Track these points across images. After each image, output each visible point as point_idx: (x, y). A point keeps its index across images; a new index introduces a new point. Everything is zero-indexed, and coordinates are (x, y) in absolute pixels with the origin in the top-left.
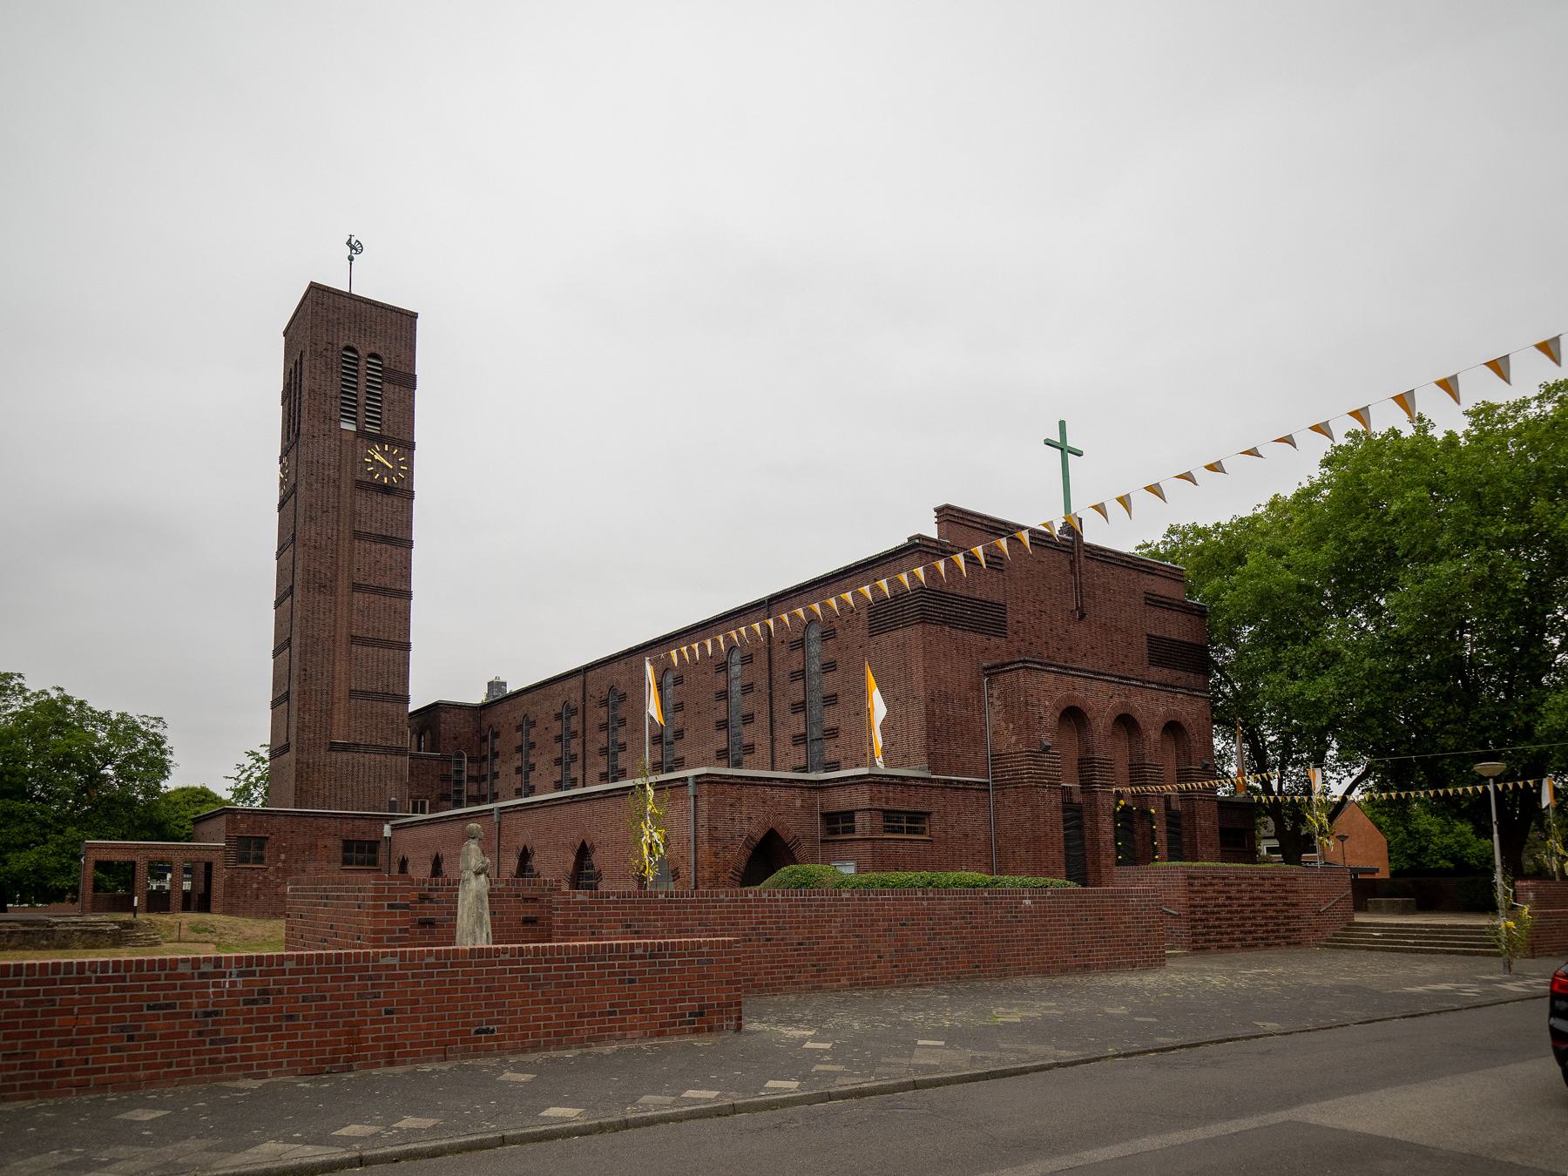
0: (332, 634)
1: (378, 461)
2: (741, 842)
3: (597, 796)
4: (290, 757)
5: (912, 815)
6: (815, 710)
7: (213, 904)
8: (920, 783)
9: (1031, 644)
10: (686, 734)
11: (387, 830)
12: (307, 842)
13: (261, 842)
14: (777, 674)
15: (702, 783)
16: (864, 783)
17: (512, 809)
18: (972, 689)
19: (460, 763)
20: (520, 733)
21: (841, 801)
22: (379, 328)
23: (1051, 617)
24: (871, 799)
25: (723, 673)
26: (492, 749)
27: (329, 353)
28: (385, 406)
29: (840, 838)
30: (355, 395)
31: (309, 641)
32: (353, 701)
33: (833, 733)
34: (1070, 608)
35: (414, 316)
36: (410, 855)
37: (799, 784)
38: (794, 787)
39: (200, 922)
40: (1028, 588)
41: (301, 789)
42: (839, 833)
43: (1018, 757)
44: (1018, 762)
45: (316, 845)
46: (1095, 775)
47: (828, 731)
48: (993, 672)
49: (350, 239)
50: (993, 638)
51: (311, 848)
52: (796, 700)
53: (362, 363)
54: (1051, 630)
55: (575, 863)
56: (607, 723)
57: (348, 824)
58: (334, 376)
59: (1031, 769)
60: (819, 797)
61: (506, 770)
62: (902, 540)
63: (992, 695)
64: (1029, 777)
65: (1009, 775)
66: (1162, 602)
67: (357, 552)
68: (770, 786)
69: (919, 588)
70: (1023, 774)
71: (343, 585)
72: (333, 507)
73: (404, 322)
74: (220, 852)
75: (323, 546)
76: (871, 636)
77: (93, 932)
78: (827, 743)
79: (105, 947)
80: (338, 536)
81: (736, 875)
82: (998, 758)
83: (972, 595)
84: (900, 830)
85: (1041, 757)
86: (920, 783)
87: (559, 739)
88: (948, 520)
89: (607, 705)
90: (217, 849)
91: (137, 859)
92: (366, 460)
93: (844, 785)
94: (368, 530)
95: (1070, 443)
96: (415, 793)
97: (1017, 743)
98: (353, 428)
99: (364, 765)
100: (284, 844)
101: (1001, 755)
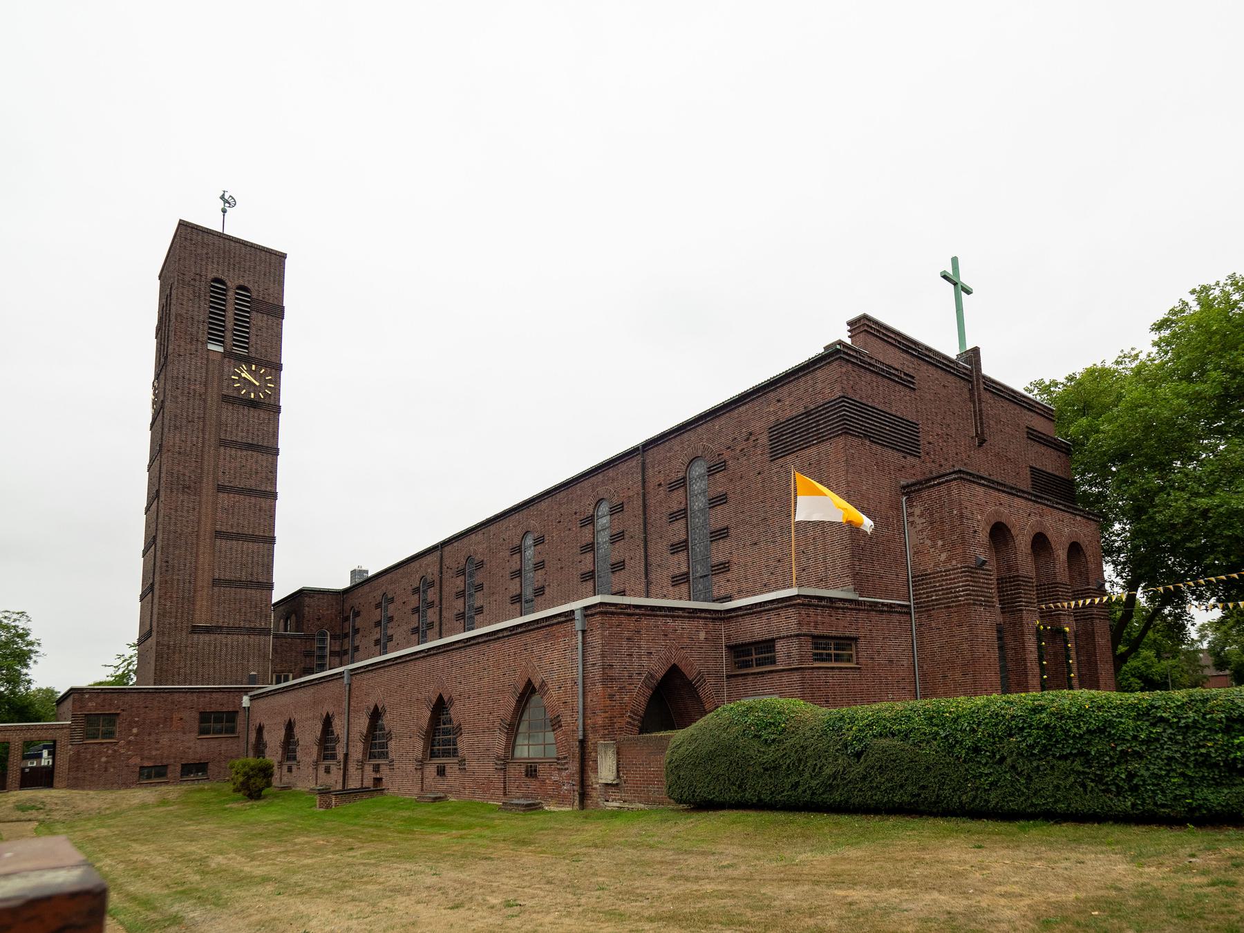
0: (196, 529)
1: (245, 378)
2: (639, 682)
3: (457, 646)
4: (152, 641)
5: (842, 642)
6: (698, 548)
7: (56, 780)
8: (847, 605)
9: (941, 466)
10: (547, 590)
11: (246, 701)
13: (111, 718)
14: (653, 517)
15: (592, 615)
16: (789, 606)
17: (363, 670)
19: (324, 641)
20: (379, 610)
21: (756, 629)
22: (248, 264)
23: (956, 441)
24: (799, 623)
25: (590, 527)
26: (353, 627)
27: (197, 283)
29: (753, 671)
30: (223, 321)
31: (172, 536)
32: (216, 589)
33: (724, 567)
35: (283, 256)
36: (267, 723)
37: (703, 615)
38: (698, 618)
39: (31, 799)
40: (936, 411)
41: (161, 669)
43: (950, 575)
44: (951, 579)
46: (1021, 593)
47: (717, 566)
48: (910, 491)
49: (224, 195)
50: (909, 457)
52: (676, 540)
53: (231, 293)
54: (957, 454)
55: (431, 719)
56: (464, 591)
58: (202, 304)
59: (969, 585)
60: (723, 628)
62: (820, 350)
64: (967, 595)
65: (936, 595)
66: (1040, 438)
67: (222, 457)
68: (673, 617)
69: (840, 398)
70: (959, 592)
71: (208, 487)
72: (199, 418)
73: (275, 261)
74: (65, 731)
75: (188, 452)
76: (772, 461)
78: (715, 579)
80: (203, 443)
81: (634, 720)
82: (921, 579)
84: (828, 658)
85: (977, 573)
86: (847, 605)
88: (865, 330)
89: (464, 574)
90: (62, 727)
92: (233, 377)
93: (761, 611)
94: (234, 439)
95: (964, 279)
96: (278, 668)
97: (949, 559)
98: (221, 349)
99: (226, 645)
100: (136, 719)
101: (926, 575)
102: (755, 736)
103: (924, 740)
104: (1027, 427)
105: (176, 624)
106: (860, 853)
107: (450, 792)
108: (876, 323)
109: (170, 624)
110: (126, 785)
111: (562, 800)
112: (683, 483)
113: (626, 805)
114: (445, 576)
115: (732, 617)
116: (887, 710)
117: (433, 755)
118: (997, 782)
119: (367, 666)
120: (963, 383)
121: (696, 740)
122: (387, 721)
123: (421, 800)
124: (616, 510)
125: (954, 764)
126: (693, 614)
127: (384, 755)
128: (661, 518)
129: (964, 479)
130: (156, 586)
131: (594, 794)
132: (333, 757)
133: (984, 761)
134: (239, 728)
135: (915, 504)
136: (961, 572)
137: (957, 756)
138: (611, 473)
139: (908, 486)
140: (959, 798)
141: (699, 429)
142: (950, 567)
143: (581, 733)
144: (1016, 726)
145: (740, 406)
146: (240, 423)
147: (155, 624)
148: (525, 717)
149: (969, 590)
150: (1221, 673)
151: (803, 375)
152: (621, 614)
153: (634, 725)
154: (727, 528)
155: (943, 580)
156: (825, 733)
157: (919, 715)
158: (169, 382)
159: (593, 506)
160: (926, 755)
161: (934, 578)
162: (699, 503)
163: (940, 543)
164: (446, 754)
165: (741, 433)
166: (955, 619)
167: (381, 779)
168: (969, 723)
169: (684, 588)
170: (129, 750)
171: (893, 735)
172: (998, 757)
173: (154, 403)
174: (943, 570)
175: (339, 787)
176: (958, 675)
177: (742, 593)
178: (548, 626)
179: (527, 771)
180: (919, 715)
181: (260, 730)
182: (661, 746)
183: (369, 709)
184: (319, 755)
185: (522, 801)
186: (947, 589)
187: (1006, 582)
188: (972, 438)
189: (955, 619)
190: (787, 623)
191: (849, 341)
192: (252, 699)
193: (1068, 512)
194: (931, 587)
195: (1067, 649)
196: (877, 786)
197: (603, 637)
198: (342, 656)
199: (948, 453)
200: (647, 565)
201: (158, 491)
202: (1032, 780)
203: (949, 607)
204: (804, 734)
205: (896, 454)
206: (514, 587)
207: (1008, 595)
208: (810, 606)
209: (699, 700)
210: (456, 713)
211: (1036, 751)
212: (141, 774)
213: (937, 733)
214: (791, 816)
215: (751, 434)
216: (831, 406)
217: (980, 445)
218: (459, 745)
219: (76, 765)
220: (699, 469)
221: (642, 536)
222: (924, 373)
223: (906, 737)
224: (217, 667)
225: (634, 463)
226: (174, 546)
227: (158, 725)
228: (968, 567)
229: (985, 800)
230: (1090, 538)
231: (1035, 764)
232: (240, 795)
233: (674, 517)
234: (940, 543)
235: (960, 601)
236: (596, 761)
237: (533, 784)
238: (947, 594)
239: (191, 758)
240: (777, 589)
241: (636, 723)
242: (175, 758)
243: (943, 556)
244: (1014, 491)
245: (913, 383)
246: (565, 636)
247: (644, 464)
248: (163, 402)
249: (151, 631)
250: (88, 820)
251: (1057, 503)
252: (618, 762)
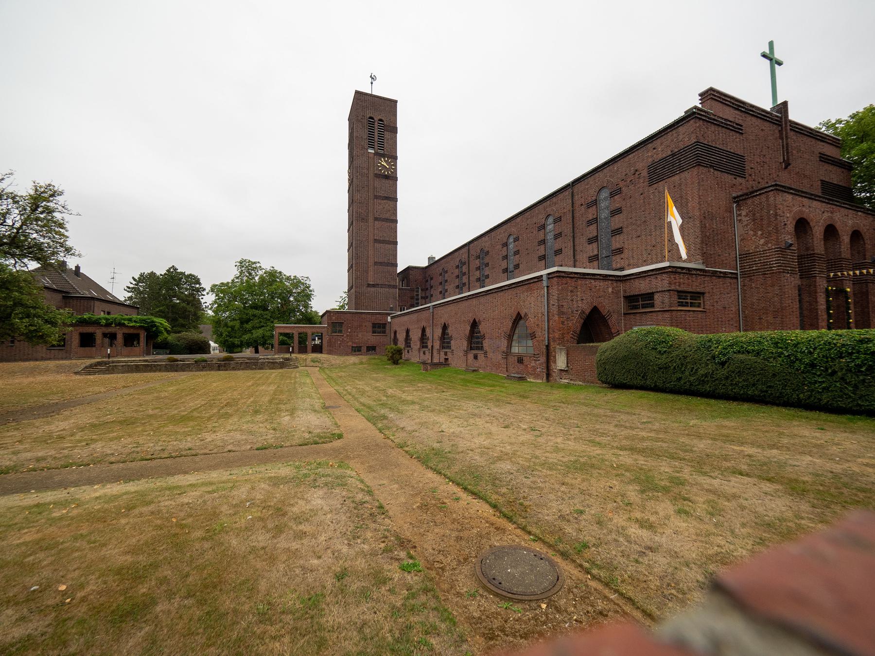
4: (353, 290)
6: (603, 239)
8: (698, 272)
9: (759, 183)
10: (521, 265)
14: (578, 223)
15: (552, 278)
16: (664, 273)
18: (726, 211)
19: (418, 291)
21: (642, 287)
24: (670, 283)
25: (543, 231)
28: (385, 141)
33: (620, 251)
34: (780, 161)
35: (396, 102)
37: (611, 278)
38: (608, 280)
42: (639, 308)
43: (766, 253)
44: (767, 256)
48: (739, 200)
50: (738, 178)
52: (591, 236)
53: (376, 123)
60: (621, 286)
61: (435, 292)
62: (682, 114)
63: (740, 215)
64: (779, 266)
65: (756, 267)
68: (594, 279)
71: (371, 219)
77: (272, 363)
78: (614, 258)
81: (574, 336)
82: (745, 256)
83: (725, 149)
84: (686, 305)
85: (786, 252)
87: (458, 277)
88: (711, 98)
89: (479, 258)
90: (324, 327)
91: (294, 332)
93: (646, 276)
95: (777, 55)
97: (766, 243)
98: (373, 152)
101: (749, 253)
102: (653, 348)
103: (772, 357)
104: (820, 153)
106: (733, 424)
107: (480, 368)
108: (718, 92)
110: (347, 354)
111: (537, 376)
112: (595, 203)
113: (572, 382)
114: (471, 259)
115: (627, 280)
116: (743, 337)
117: (471, 349)
118: (828, 388)
119: (453, 300)
120: (775, 126)
121: (615, 349)
122: (450, 331)
123: (467, 370)
124: (558, 220)
125: (795, 373)
126: (605, 277)
127: (449, 347)
128: (582, 224)
129: (779, 190)
130: (354, 265)
131: (554, 374)
132: (427, 347)
133: (818, 373)
134: (387, 331)
135: (742, 208)
136: (775, 251)
137: (797, 368)
138: (554, 200)
139: (738, 197)
140: (798, 395)
141: (605, 170)
142: (767, 248)
143: (547, 342)
144: (846, 352)
145: (630, 154)
146: (382, 185)
147: (354, 283)
148: (517, 331)
149: (780, 263)
150: (392, 340)
151: (671, 131)
152: (567, 277)
153: (574, 339)
154: (622, 228)
155: (761, 257)
156: (699, 348)
157: (767, 341)
158: (355, 170)
159: (544, 219)
160: (773, 366)
161: (755, 255)
162: (604, 214)
163: (760, 233)
164: (478, 348)
165: (630, 170)
166: (769, 282)
167: (448, 359)
168: (807, 348)
169: (596, 263)
171: (748, 352)
172: (830, 371)
173: (349, 180)
174: (761, 250)
175: (429, 361)
176: (770, 318)
177: (630, 266)
178: (529, 284)
179: (518, 360)
180: (767, 341)
181: (395, 332)
182: (594, 351)
183: (470, 322)
184: (420, 346)
185: (516, 375)
186: (764, 262)
187: (805, 258)
188: (780, 163)
189: (769, 282)
190: (662, 283)
191: (700, 106)
192: (392, 318)
193: (851, 209)
194: (752, 262)
195: (848, 303)
196: (736, 384)
197: (558, 290)
198: (427, 299)
199: (764, 175)
200: (574, 250)
201: (352, 221)
202: (858, 389)
203: (765, 274)
204: (685, 349)
205: (730, 176)
206: (504, 265)
207: (805, 266)
208: (676, 273)
209: (608, 327)
210: (483, 328)
211: (863, 369)
213: (782, 353)
214: (677, 397)
215: (636, 171)
216: (689, 149)
217: (786, 168)
218: (484, 345)
220: (605, 194)
221: (572, 235)
222: (749, 123)
223: (758, 354)
225: (567, 193)
228: (780, 248)
229: (818, 399)
230: (868, 227)
231: (861, 378)
232: (389, 362)
233: (590, 223)
234: (760, 233)
235: (773, 270)
236: (555, 357)
237: (521, 367)
238: (764, 265)
239: (370, 344)
240: (652, 263)
241: (575, 338)
243: (762, 241)
244: (812, 197)
245: (742, 130)
246: (537, 289)
247: (572, 193)
248: (352, 179)
249: (352, 286)
250: (336, 368)
251: (844, 204)
252: (567, 358)
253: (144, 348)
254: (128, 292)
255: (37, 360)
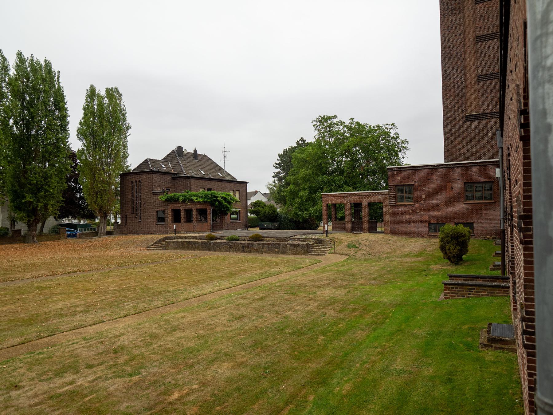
0: (462, 40)
12: (439, 186)
32: (480, 83)
45: (446, 187)
51: (442, 190)
57: (467, 170)
79: (301, 254)
91: (345, 202)
99: (491, 127)
100: (424, 188)
105: (455, 116)
109: (451, 117)
170: (421, 210)
212: (430, 229)
219: (393, 219)
224: (486, 146)
226: (449, 58)
227: (437, 193)
242: (450, 218)
253: (210, 223)
254: (276, 168)
255: (151, 233)
